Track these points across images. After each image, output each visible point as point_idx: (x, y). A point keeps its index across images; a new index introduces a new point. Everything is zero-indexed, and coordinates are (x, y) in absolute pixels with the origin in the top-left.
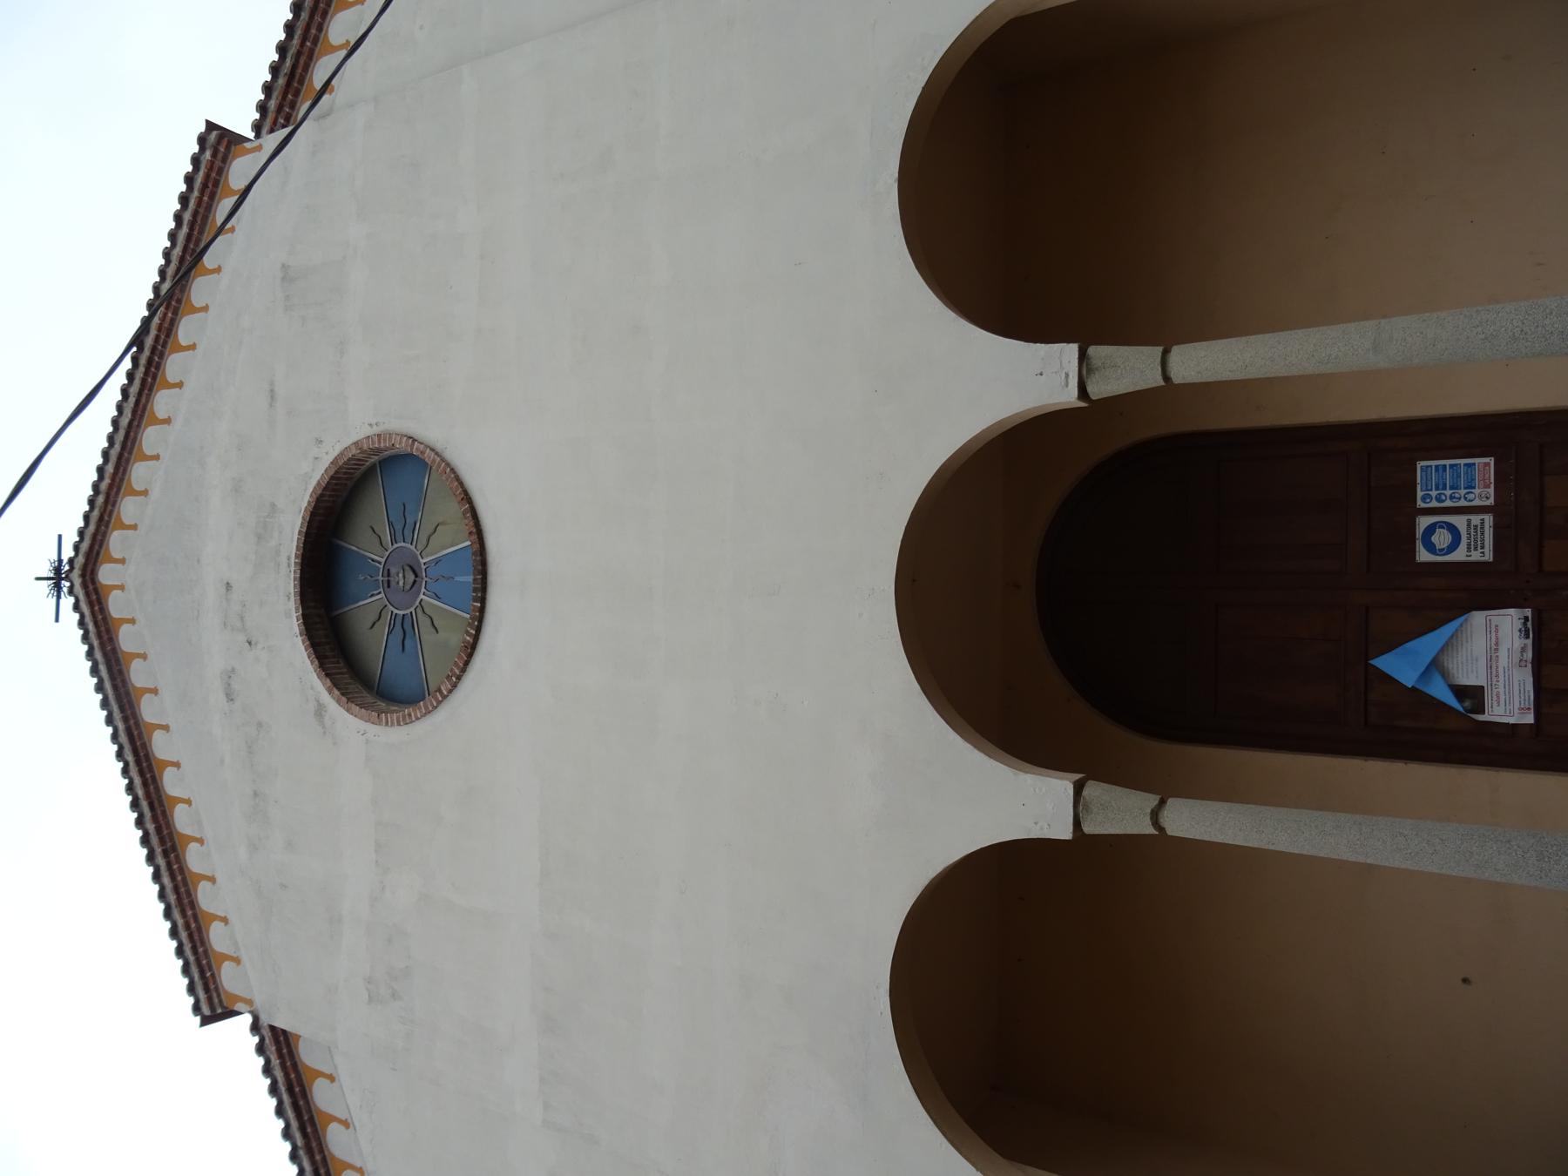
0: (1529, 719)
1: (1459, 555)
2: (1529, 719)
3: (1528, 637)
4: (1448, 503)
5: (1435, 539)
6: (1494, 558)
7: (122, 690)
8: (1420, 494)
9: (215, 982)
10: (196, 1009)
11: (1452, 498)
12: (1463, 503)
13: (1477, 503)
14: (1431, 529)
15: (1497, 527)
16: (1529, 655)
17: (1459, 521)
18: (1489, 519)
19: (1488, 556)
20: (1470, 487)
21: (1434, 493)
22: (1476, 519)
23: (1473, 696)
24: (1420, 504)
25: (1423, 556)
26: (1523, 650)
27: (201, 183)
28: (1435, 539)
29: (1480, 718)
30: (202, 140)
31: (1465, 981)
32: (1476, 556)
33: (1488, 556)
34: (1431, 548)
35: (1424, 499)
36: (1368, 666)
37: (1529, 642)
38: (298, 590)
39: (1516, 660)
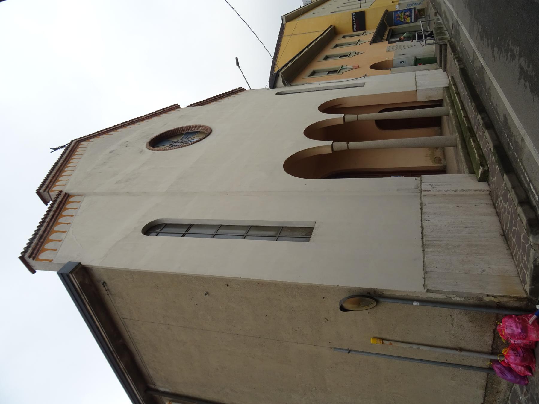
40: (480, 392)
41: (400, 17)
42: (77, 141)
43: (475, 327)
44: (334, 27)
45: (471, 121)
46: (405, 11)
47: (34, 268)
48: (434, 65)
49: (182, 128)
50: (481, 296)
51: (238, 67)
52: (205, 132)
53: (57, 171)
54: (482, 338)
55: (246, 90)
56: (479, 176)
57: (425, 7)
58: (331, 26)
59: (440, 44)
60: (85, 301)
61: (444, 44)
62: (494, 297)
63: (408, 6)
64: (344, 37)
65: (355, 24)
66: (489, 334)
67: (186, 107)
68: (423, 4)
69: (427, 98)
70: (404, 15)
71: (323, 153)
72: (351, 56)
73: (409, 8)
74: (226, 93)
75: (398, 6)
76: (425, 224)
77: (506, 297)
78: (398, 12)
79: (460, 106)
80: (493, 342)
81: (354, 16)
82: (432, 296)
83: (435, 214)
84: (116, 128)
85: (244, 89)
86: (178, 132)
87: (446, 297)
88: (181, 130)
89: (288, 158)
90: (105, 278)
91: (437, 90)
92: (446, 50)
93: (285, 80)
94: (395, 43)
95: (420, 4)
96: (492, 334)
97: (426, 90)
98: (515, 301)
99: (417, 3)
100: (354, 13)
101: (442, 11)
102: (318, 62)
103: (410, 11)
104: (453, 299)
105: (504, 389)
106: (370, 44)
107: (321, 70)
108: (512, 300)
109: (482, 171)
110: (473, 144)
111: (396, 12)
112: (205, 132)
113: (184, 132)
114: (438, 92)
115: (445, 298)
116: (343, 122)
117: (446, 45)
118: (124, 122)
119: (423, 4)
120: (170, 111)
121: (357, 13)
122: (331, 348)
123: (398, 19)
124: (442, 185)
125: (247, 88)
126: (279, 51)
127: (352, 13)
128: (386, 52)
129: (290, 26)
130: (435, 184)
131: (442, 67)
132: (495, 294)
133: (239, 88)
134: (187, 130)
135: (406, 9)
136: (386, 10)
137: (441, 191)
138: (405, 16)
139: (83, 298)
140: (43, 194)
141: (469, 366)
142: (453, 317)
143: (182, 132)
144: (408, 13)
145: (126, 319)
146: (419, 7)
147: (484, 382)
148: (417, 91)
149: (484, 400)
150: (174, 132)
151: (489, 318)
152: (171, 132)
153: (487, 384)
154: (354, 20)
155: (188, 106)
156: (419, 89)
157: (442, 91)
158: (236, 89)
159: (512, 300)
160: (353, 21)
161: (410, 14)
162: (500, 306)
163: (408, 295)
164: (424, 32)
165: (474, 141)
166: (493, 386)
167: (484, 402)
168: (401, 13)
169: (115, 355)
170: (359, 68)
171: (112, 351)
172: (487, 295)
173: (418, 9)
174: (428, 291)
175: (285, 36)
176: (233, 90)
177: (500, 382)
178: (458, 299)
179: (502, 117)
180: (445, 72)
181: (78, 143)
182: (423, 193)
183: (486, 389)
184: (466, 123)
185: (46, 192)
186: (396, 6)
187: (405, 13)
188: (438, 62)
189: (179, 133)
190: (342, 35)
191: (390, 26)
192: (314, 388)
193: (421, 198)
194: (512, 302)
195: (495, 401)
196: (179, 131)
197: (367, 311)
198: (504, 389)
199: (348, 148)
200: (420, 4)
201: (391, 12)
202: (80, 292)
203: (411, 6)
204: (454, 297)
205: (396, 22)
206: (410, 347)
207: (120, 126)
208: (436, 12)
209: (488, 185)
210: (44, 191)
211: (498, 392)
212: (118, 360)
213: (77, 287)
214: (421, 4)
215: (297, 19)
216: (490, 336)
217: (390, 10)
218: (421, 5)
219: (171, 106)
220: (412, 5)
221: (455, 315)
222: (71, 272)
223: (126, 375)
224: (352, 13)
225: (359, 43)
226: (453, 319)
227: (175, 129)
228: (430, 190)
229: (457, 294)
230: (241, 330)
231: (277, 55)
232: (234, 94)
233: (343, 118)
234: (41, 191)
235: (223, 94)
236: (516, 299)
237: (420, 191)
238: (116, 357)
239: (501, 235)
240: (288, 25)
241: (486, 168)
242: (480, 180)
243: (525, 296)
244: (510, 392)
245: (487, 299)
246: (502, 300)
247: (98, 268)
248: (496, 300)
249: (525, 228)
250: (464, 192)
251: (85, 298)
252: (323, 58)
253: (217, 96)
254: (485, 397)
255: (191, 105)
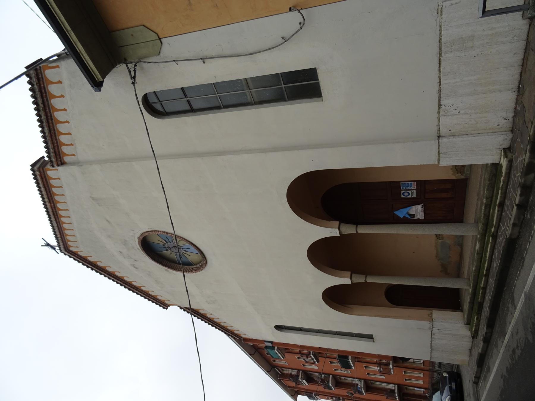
0: (423, 218)
1: (410, 196)
2: (423, 218)
3: (423, 208)
4: (407, 189)
5: (405, 194)
6: (416, 195)
7: (99, 268)
8: (401, 187)
9: (165, 303)
10: (164, 308)
11: (408, 188)
12: (410, 189)
13: (413, 189)
14: (404, 193)
15: (417, 192)
16: (423, 210)
17: (410, 192)
18: (415, 191)
19: (415, 196)
20: (411, 186)
21: (404, 187)
22: (413, 191)
23: (414, 216)
24: (401, 189)
25: (403, 196)
26: (422, 210)
27: (40, 179)
28: (405, 194)
29: (415, 218)
30: (32, 170)
31: (414, 252)
32: (413, 196)
33: (415, 196)
34: (404, 195)
35: (402, 188)
36: (393, 212)
37: (423, 209)
38: (146, 254)
39: (421, 211)
45: (517, 76)
67: (174, 309)
76: (432, 342)
79: (485, 269)
83: (439, 339)
110: (475, 320)
124: (445, 330)
130: (442, 329)
165: (477, 319)
184: (481, 297)
219: (145, 298)
234: (36, 168)
239: (470, 350)
249: (486, 322)
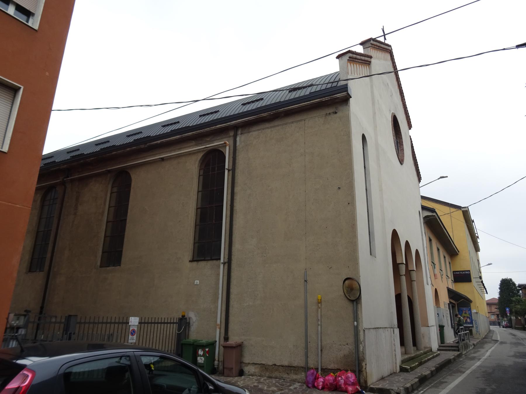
40: (286, 363)
41: (465, 313)
42: (390, 51)
43: (340, 358)
44: (458, 254)
46: (471, 318)
47: (340, 58)
48: (440, 342)
49: (402, 138)
50: (365, 361)
51: (439, 177)
52: (401, 162)
53: (378, 46)
54: (332, 363)
55: (419, 183)
56: (403, 366)
57: (474, 335)
58: (459, 252)
59: (459, 346)
60: (323, 98)
61: (459, 349)
62: (366, 368)
63: (475, 321)
64: (450, 263)
65: (460, 273)
66: (336, 367)
68: (477, 334)
69: (423, 334)
70: (467, 317)
71: (397, 257)
72: (440, 271)
73: (473, 321)
74: (418, 167)
75: (476, 312)
77: (367, 375)
78: (470, 312)
80: (329, 369)
81: (467, 272)
82: (361, 333)
84: (398, 80)
85: (420, 182)
86: (398, 136)
87: (361, 341)
88: (399, 137)
89: (396, 231)
90: (339, 114)
91: (429, 342)
92: (454, 350)
93: (430, 218)
94: (449, 309)
95: (477, 331)
96: (336, 368)
97: (429, 334)
98: (365, 380)
99: (477, 329)
100: (470, 273)
101: (479, 349)
102: (436, 243)
103: (470, 322)
104: (361, 345)
105: (292, 377)
106: (447, 287)
107: (432, 247)
108: (364, 377)
109: (407, 368)
111: (470, 310)
112: (401, 162)
113: (398, 140)
114: (428, 343)
115: (360, 340)
116: (410, 270)
117: (459, 351)
118: (402, 86)
119: (477, 334)
120: (408, 122)
121: (469, 275)
122: (306, 269)
123: (464, 312)
125: (421, 184)
126: (436, 203)
127: (469, 271)
128: (444, 302)
129: (459, 214)
131: (439, 347)
132: (367, 369)
133: (421, 177)
134: (400, 142)
135: (473, 319)
136: (472, 302)
137: (394, 341)
138: (466, 318)
139: (326, 98)
140: (369, 43)
141: (307, 355)
142: (347, 345)
143: (398, 138)
144: (468, 320)
145: (305, 123)
146: (474, 330)
147: (295, 364)
148: (428, 327)
149: (279, 366)
150: (399, 132)
151: (349, 366)
152: (399, 130)
153: (294, 367)
154: (464, 273)
155: (410, 136)
156: (429, 329)
157: (428, 346)
158: (420, 175)
159: (364, 377)
160: (463, 271)
161: (468, 322)
162: (360, 371)
163: (359, 319)
164: (464, 334)
166: (293, 371)
167: (277, 366)
168: (469, 314)
169: (274, 111)
170: (435, 279)
171: (278, 110)
172: (366, 364)
173: (473, 330)
174: (364, 330)
175: (450, 209)
176: (420, 172)
177: (297, 375)
178: (361, 348)
179: (445, 380)
180: (437, 350)
181: (390, 51)
182: (392, 329)
183: (289, 366)
185: (371, 45)
186: (475, 310)
187: (469, 318)
188: (442, 345)
189: (397, 136)
190: (450, 262)
191: (457, 304)
192: (265, 255)
193: (390, 328)
194: (364, 378)
195: (280, 372)
196: (399, 136)
197: (343, 294)
198: (292, 377)
199: (401, 275)
200: (477, 331)
201: (470, 306)
202: (331, 97)
203: (476, 324)
204: (362, 345)
205: (461, 310)
206: (319, 320)
207: (400, 83)
208: (475, 345)
209: (368, 377)
210: (371, 44)
211: (288, 373)
212: (269, 113)
213: (335, 95)
214: (477, 332)
215: (464, 221)
216: (335, 367)
217: (472, 305)
218: (476, 332)
220: (476, 324)
221: (348, 346)
222: (348, 94)
223: (255, 116)
224: (469, 271)
225: (447, 277)
226: (345, 345)
227: (401, 133)
228: (394, 334)
229: (364, 347)
230: (310, 208)
231: (430, 200)
232: (417, 173)
233: (413, 270)
235: (418, 165)
236: (365, 380)
237: (392, 327)
238: (273, 112)
240: (460, 213)
241: (409, 370)
242: (400, 367)
243: (368, 385)
244: (290, 381)
245: (364, 364)
246: (364, 372)
247: (349, 110)
248: (363, 369)
250: (394, 356)
251: (325, 99)
252: (438, 247)
253: (416, 160)
254: (281, 366)
255: (411, 139)
